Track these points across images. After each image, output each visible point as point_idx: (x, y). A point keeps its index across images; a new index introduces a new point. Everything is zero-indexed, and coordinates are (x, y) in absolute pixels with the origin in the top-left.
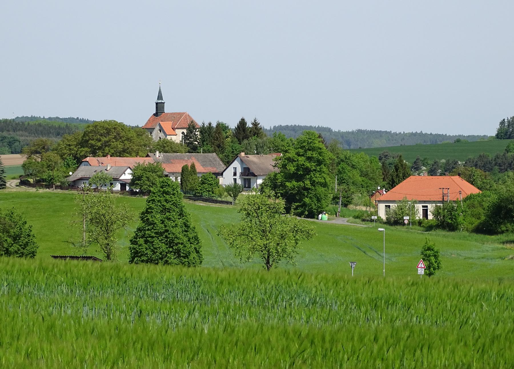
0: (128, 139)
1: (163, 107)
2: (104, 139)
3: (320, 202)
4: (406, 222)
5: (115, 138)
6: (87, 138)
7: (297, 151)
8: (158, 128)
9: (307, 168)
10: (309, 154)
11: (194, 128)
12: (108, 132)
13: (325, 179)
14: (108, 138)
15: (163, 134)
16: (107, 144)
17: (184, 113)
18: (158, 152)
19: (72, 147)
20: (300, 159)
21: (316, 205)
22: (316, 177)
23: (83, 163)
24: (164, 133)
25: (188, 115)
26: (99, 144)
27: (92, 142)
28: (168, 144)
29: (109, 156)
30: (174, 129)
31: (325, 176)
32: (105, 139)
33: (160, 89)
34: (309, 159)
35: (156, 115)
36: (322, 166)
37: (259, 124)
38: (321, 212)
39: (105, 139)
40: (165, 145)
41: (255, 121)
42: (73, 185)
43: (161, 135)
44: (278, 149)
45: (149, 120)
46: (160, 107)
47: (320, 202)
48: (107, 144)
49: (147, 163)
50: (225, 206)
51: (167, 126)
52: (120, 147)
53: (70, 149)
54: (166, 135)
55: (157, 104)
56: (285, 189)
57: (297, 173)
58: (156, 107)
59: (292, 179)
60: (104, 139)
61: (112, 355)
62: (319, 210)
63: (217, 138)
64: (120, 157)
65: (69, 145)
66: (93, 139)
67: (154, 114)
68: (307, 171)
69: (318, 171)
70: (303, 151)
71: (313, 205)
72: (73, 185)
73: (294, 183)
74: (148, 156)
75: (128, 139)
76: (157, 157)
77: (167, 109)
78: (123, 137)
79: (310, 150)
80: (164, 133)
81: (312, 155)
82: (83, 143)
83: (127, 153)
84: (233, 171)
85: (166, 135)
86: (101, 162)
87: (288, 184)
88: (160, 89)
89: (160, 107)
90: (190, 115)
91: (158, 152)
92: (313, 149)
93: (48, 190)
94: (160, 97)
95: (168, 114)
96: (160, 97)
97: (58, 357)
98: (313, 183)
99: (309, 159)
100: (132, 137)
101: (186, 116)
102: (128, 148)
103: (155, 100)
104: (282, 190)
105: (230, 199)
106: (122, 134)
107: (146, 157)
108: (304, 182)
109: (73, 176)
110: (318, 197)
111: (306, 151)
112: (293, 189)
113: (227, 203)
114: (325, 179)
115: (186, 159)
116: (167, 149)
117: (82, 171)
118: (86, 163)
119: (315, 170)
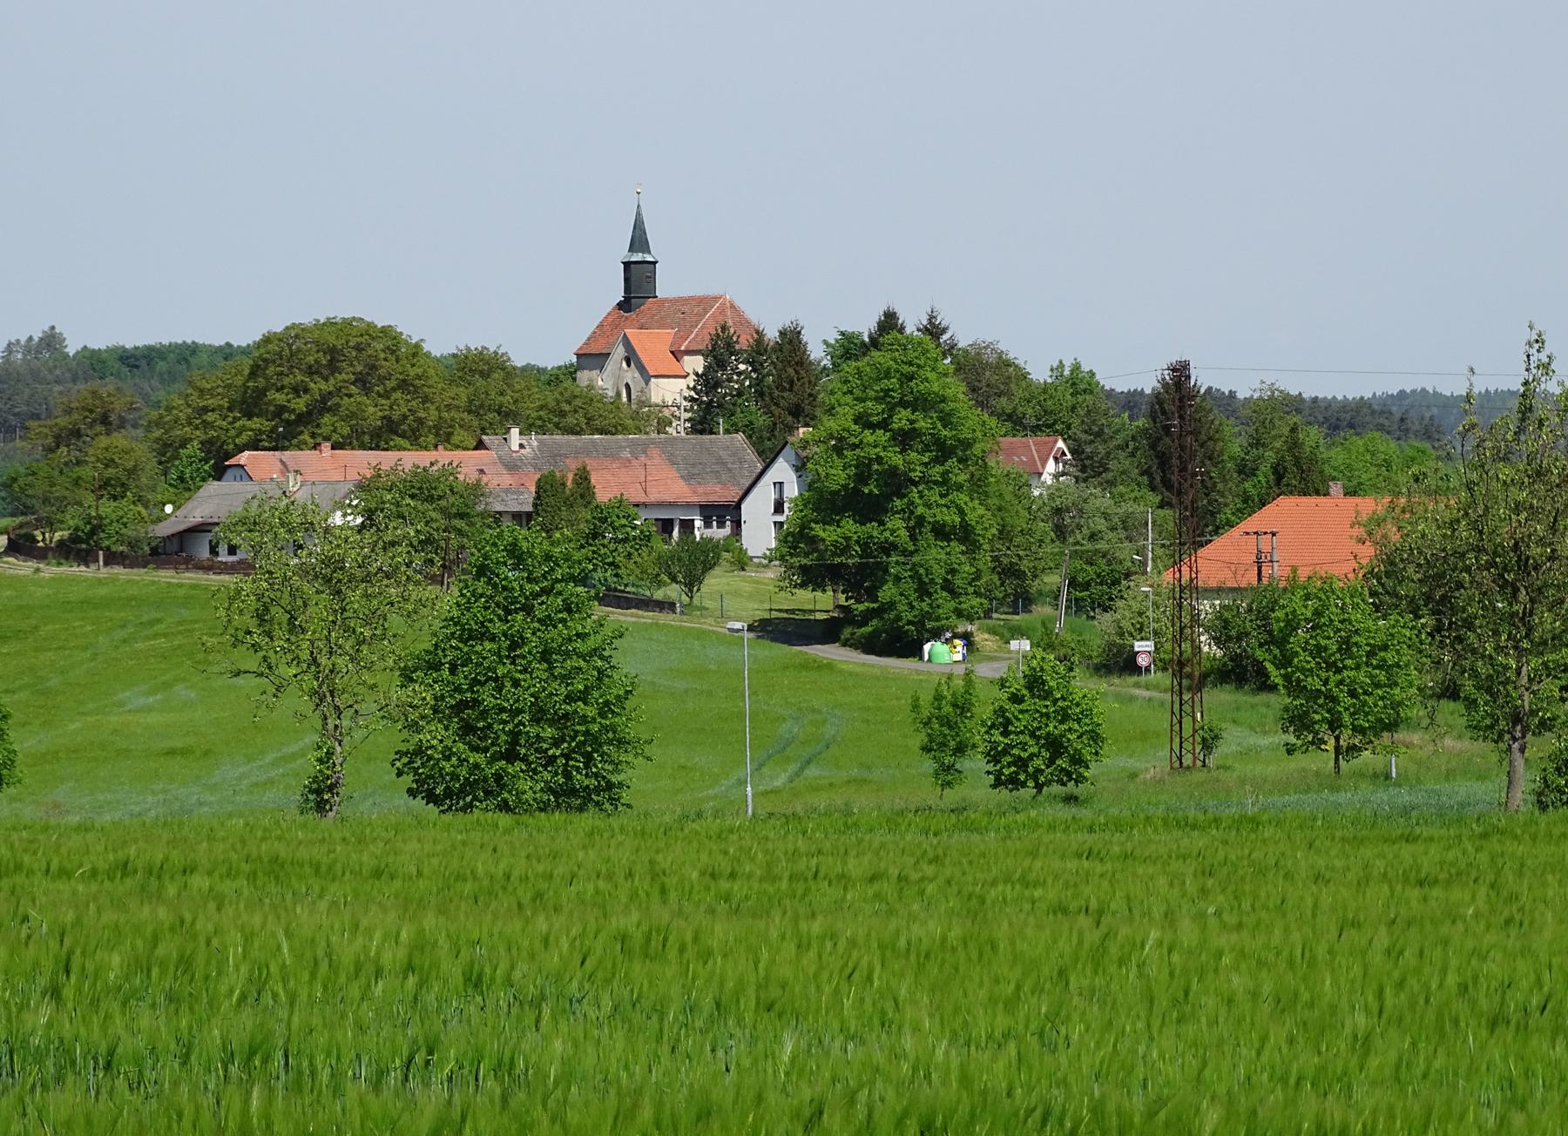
0: (404, 385)
1: (652, 279)
2: (319, 386)
3: (930, 595)
4: (1142, 661)
5: (362, 381)
6: (261, 382)
7: (859, 408)
8: (619, 352)
9: (893, 472)
10: (902, 418)
11: (729, 345)
12: (334, 358)
13: (961, 512)
14: (332, 381)
15: (637, 374)
16: (323, 405)
17: (716, 299)
18: (515, 432)
19: (210, 417)
20: (868, 436)
21: (912, 607)
22: (929, 506)
23: (230, 474)
24: (642, 369)
25: (732, 306)
26: (300, 404)
27: (280, 398)
28: (578, 402)
29: (326, 446)
30: (677, 355)
31: (962, 498)
32: (323, 386)
33: (639, 214)
34: (905, 439)
35: (625, 305)
36: (952, 462)
37: (944, 330)
38: (936, 635)
39: (323, 386)
40: (567, 408)
41: (931, 318)
42: (174, 550)
43: (631, 376)
44: (1055, 422)
45: (601, 326)
46: (638, 280)
47: (930, 595)
48: (323, 405)
49: (408, 467)
50: (664, 618)
51: (652, 343)
52: (373, 412)
53: (206, 424)
54: (647, 377)
55: (627, 265)
56: (817, 550)
57: (856, 491)
58: (626, 280)
59: (841, 511)
60: (319, 386)
61: (1204, 1019)
62: (929, 625)
63: (792, 383)
64: (377, 448)
65: (205, 410)
66: (283, 387)
67: (620, 306)
68: (897, 483)
69: (936, 483)
70: (880, 408)
71: (901, 607)
72: (174, 550)
73: (849, 526)
74: (480, 445)
75: (404, 385)
76: (515, 447)
77: (667, 286)
78: (389, 377)
79: (904, 404)
80: (642, 369)
81: (912, 422)
82: (250, 404)
83: (403, 436)
84: (772, 496)
85: (647, 377)
86: (291, 465)
87: (818, 530)
88: (639, 214)
89: (638, 280)
90: (737, 303)
91: (515, 432)
92: (921, 403)
93: (83, 568)
94: (639, 241)
95: (666, 300)
96: (639, 241)
97: (249, 1093)
98: (916, 526)
99: (905, 439)
100: (419, 377)
101: (722, 310)
102: (405, 417)
103: (623, 253)
104: (807, 555)
105: (673, 591)
106: (386, 366)
107: (476, 448)
108: (882, 523)
109: (175, 517)
110: (920, 579)
111: (891, 410)
112: (845, 550)
113: (667, 606)
114: (961, 512)
115: (626, 454)
116: (570, 420)
117: (213, 501)
118: (238, 472)
119: (924, 479)
